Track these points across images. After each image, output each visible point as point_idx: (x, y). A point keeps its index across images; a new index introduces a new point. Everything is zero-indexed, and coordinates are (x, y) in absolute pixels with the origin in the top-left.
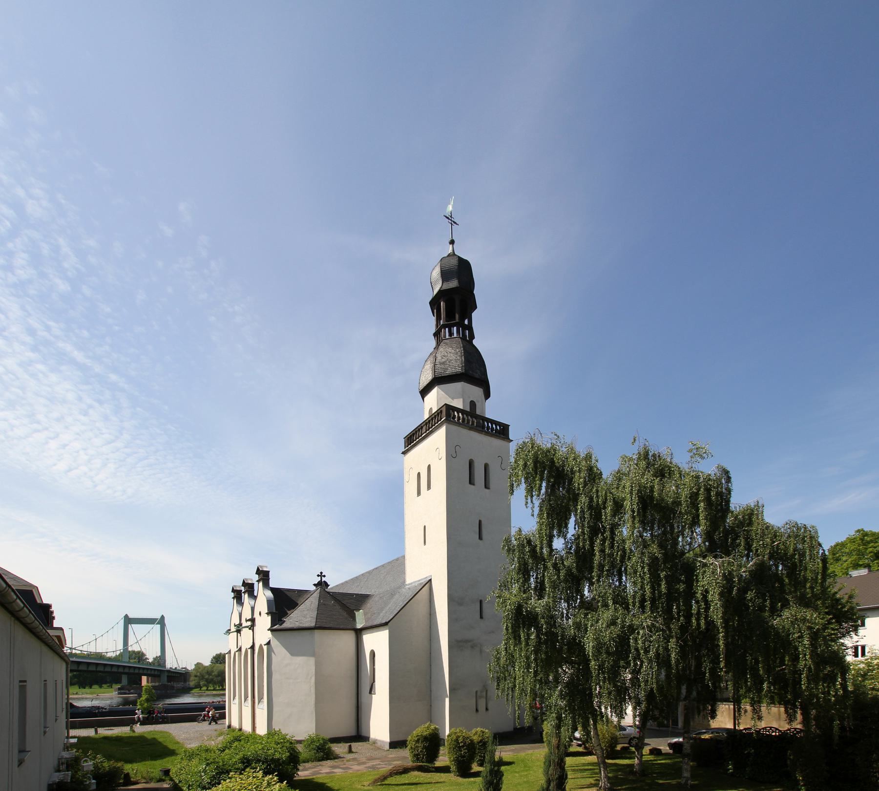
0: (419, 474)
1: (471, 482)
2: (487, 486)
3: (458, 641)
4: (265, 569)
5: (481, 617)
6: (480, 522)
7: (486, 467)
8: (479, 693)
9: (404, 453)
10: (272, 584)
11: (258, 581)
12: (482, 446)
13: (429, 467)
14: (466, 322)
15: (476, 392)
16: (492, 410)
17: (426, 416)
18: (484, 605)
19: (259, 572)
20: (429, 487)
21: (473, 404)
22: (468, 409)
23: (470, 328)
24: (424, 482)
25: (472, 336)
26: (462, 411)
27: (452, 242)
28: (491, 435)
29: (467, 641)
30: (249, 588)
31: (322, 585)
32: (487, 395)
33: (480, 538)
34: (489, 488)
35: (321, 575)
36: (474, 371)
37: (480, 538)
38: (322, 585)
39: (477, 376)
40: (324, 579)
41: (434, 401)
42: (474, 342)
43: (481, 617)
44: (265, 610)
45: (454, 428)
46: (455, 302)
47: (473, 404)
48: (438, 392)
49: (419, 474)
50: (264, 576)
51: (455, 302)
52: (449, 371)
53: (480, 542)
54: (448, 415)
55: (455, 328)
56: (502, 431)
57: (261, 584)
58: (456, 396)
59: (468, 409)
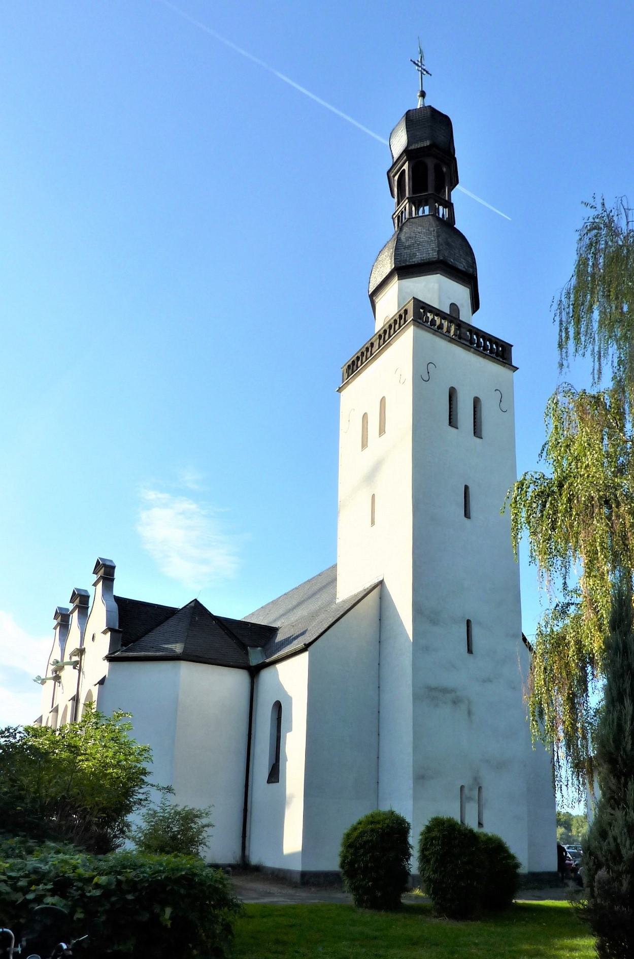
0: (365, 416)
1: (452, 421)
2: (477, 431)
3: (430, 689)
5: (470, 651)
6: (466, 488)
7: (476, 401)
8: (466, 791)
11: (95, 585)
12: (470, 370)
13: (383, 400)
15: (459, 293)
18: (475, 630)
20: (382, 431)
27: (423, 94)
28: (485, 356)
29: (445, 691)
30: (81, 600)
33: (467, 514)
34: (469, 518)
36: (456, 261)
37: (467, 514)
41: (389, 304)
43: (470, 651)
46: (429, 164)
47: (453, 306)
49: (365, 416)
50: (106, 572)
51: (429, 164)
52: (419, 257)
53: (478, 440)
57: (100, 584)
59: (447, 310)
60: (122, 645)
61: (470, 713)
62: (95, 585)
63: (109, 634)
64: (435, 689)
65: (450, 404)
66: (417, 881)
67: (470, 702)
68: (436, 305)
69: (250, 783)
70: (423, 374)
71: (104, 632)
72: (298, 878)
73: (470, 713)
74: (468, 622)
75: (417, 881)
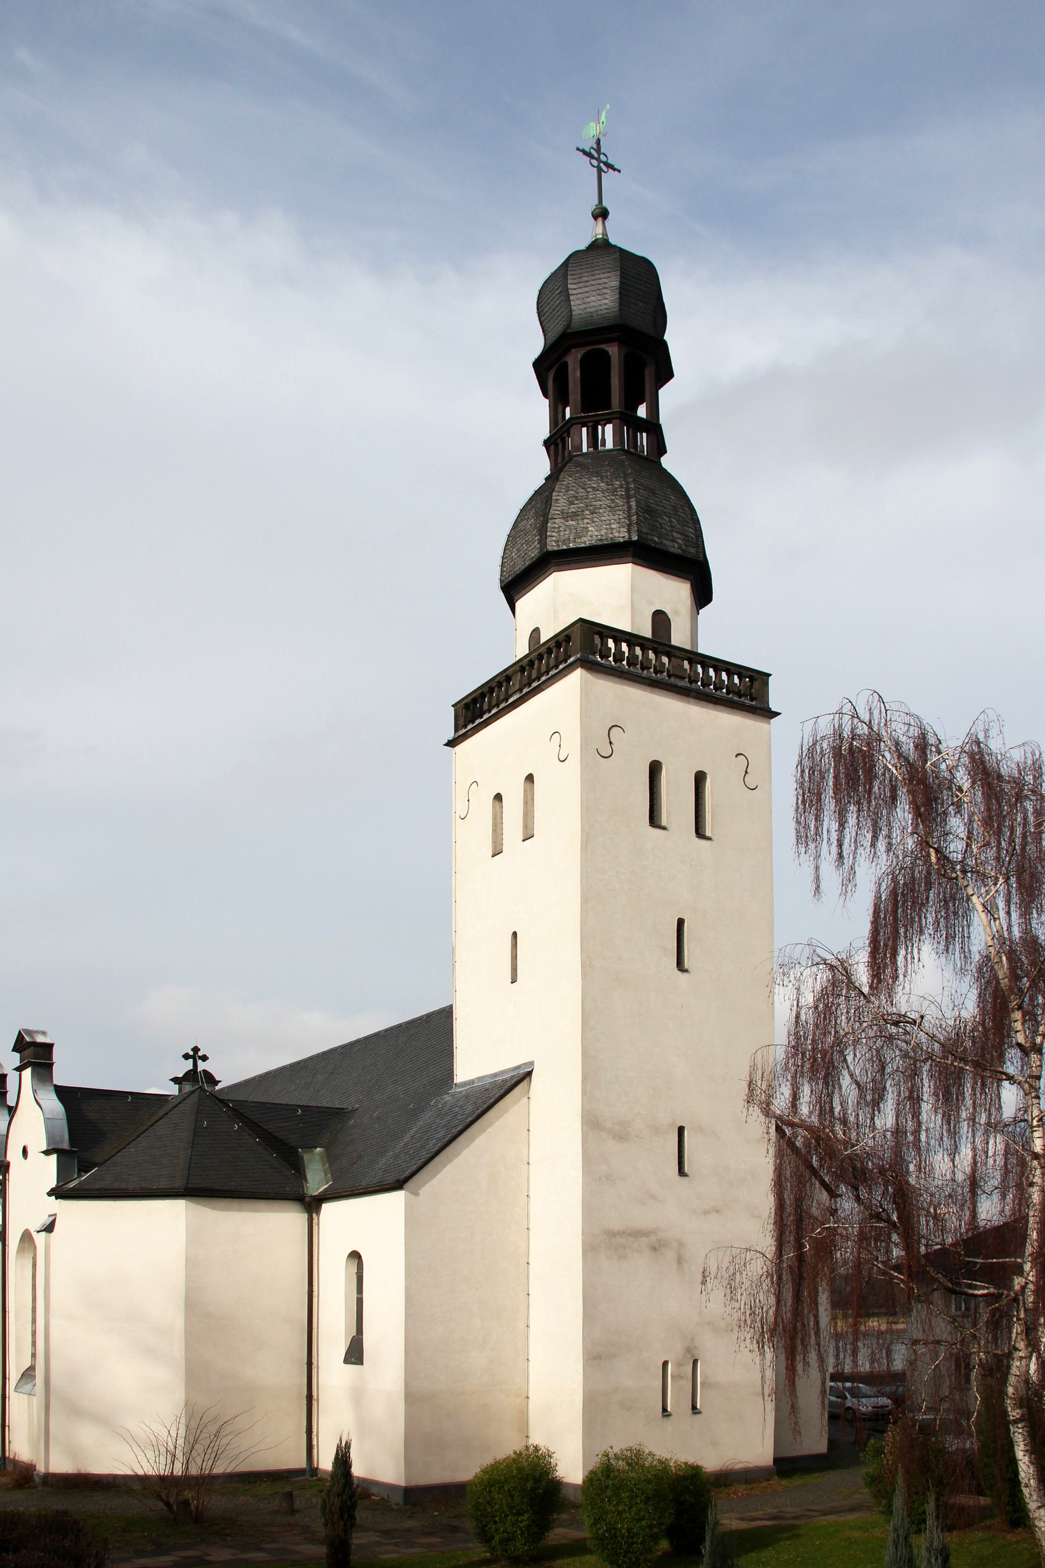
3: (612, 1234)
4: (40, 1039)
5: (682, 1172)
6: (681, 923)
9: (452, 743)
10: (64, 1075)
11: (19, 1069)
12: (688, 731)
14: (642, 411)
15: (672, 593)
16: (719, 634)
17: (522, 650)
19: (21, 1045)
21: (660, 619)
22: (647, 632)
23: (653, 427)
24: (515, 815)
25: (659, 447)
26: (632, 639)
29: (637, 1234)
31: (197, 1079)
32: (703, 595)
35: (195, 1055)
36: (670, 542)
38: (197, 1079)
39: (674, 548)
40: (202, 1066)
42: (667, 462)
44: (39, 1141)
45: (608, 689)
47: (660, 619)
48: (585, 693)
50: (36, 1055)
54: (589, 647)
55: (609, 428)
56: (744, 691)
57: (27, 1073)
58: (613, 594)
59: (647, 632)
60: (80, 1171)
61: (680, 1260)
62: (19, 1069)
63: (54, 1158)
64: (621, 1233)
65: (360, 1302)
66: (1015, 1422)
67: (681, 1244)
68: (624, 624)
69: (314, 1360)
70: (602, 744)
71: (47, 1153)
72: (398, 1499)
73: (680, 1260)
74: (681, 1130)
75: (1015, 1422)
